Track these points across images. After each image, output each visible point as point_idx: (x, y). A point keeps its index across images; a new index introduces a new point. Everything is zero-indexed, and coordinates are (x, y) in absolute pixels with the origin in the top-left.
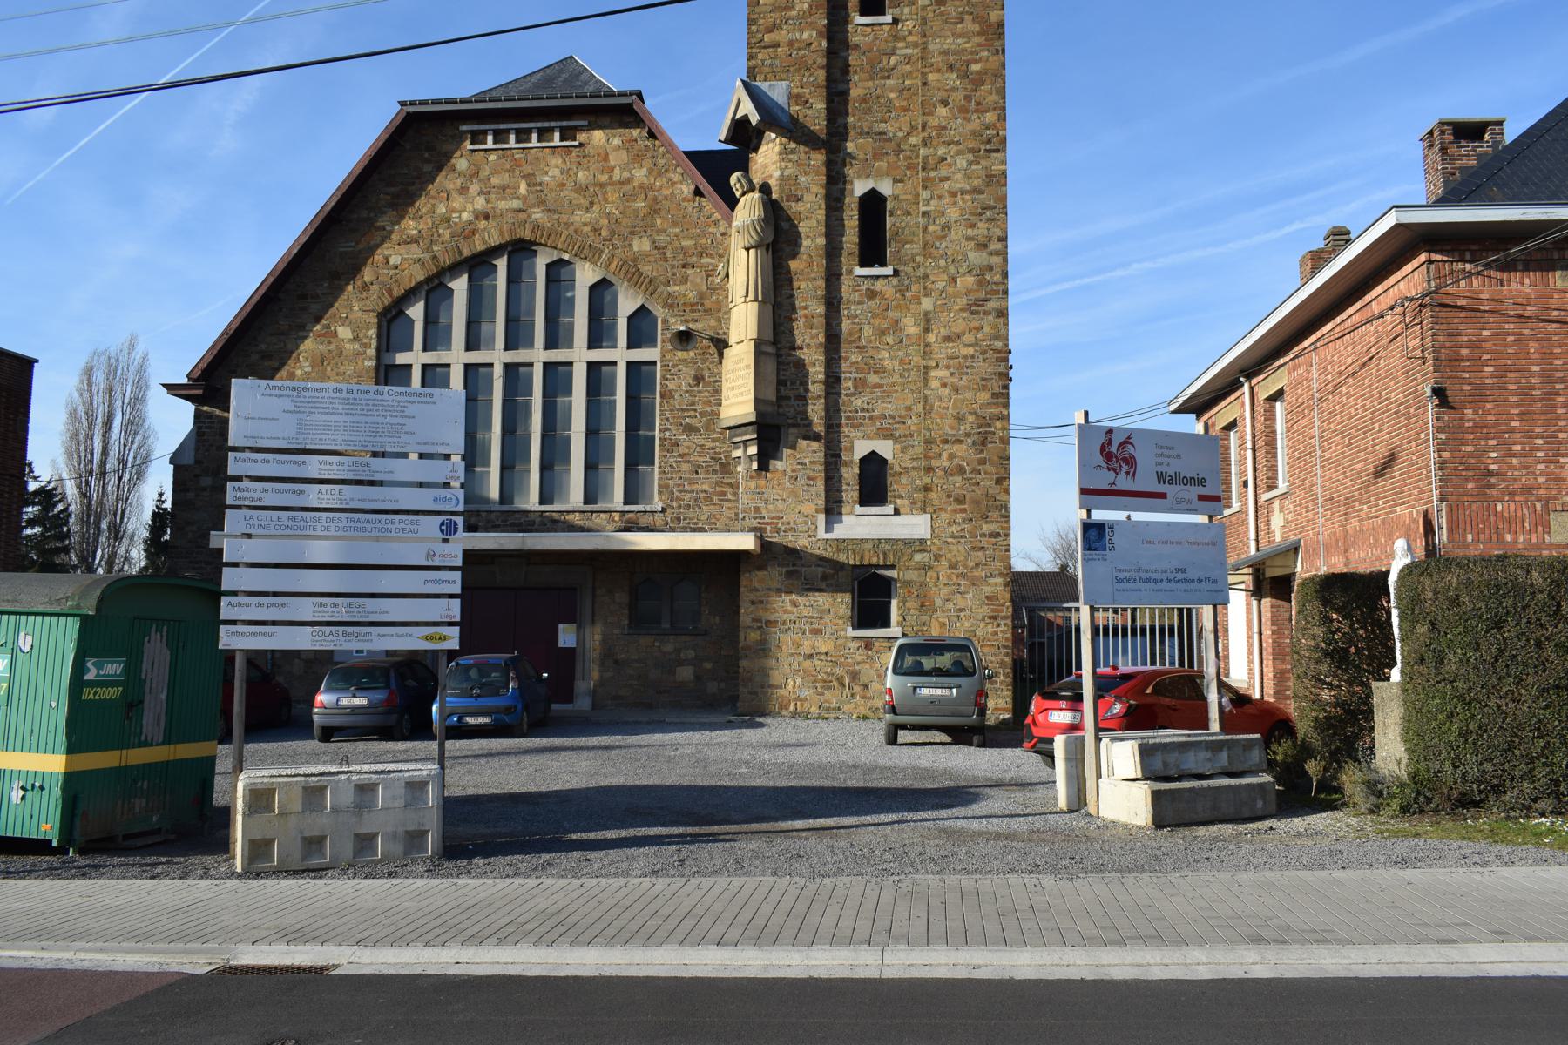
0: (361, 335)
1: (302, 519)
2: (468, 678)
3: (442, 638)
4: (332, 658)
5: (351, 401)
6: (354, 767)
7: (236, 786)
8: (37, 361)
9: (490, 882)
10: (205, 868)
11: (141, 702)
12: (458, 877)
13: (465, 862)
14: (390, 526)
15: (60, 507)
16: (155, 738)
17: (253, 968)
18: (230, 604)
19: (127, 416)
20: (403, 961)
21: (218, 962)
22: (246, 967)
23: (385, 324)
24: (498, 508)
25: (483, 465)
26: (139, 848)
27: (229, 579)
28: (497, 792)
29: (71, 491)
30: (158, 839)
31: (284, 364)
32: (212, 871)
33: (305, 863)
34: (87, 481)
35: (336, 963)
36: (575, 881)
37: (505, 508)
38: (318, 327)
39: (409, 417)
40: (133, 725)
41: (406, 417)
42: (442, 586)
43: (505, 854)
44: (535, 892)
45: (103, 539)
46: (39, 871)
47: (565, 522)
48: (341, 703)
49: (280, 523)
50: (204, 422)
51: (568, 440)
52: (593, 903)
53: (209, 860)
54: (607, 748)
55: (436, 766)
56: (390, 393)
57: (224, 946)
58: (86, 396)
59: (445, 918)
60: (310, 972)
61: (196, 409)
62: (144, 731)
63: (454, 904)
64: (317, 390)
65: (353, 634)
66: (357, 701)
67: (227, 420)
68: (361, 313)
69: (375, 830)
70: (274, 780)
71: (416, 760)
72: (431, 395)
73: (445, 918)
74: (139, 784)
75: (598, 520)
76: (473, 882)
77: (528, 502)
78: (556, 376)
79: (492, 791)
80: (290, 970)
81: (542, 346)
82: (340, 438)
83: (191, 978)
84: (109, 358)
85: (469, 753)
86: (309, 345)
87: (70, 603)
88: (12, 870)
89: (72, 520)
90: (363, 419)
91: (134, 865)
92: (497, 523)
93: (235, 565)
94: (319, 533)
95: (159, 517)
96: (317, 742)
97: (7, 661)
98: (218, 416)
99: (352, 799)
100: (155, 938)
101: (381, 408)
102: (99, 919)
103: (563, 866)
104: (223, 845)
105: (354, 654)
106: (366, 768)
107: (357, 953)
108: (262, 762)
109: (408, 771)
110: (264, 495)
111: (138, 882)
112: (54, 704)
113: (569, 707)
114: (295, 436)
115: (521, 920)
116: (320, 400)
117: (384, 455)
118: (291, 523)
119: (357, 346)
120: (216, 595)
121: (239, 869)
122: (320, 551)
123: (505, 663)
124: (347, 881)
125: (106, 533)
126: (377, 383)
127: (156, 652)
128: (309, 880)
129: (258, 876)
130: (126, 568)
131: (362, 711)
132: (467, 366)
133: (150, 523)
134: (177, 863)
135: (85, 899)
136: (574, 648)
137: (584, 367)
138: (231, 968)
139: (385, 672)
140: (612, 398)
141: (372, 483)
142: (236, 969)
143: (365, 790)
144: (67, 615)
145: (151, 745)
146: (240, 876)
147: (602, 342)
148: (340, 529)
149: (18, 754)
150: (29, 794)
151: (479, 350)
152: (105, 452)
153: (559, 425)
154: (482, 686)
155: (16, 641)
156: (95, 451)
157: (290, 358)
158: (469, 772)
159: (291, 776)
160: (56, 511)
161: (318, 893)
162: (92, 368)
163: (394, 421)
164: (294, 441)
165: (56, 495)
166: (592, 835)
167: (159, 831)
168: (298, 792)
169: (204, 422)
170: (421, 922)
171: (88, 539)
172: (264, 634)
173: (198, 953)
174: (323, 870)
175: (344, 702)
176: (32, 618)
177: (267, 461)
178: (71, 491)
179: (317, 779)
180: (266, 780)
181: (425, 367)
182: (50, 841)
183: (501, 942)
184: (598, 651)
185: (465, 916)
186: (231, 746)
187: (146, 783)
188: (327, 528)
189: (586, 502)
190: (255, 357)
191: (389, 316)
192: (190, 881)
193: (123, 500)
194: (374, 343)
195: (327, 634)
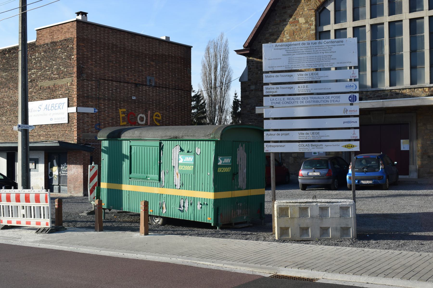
0: (308, 21)
1: (293, 99)
2: (361, 164)
3: (352, 146)
4: (304, 156)
5: (309, 48)
6: (319, 200)
7: (274, 206)
8: (192, 47)
9: (378, 250)
10: (264, 237)
11: (238, 173)
12: (364, 247)
13: (366, 242)
14: (328, 99)
15: (202, 101)
16: (243, 187)
17: (286, 277)
18: (267, 134)
19: (222, 65)
20: (345, 280)
21: (273, 273)
22: (283, 276)
23: (318, 14)
24: (371, 89)
25: (363, 71)
26: (240, 228)
27: (267, 124)
28: (377, 213)
29: (205, 95)
30: (247, 225)
31: (279, 37)
32: (267, 239)
33: (301, 238)
34: (210, 91)
35: (318, 278)
36: (417, 253)
37: (374, 89)
38: (291, 20)
39: (333, 52)
40: (235, 182)
41: (332, 52)
42: (352, 124)
43: (384, 239)
44: (399, 256)
45: (217, 113)
46: (208, 234)
47: (402, 94)
48: (309, 174)
49: (284, 101)
50: (251, 64)
51: (402, 56)
52: (427, 263)
53: (265, 234)
54: (426, 195)
55: (352, 201)
56: (325, 42)
57: (275, 267)
58: (208, 59)
59: (361, 264)
60: (308, 280)
61: (247, 59)
62: (239, 184)
63: (363, 258)
64: (295, 45)
65: (315, 145)
66: (316, 174)
67: (261, 63)
68: (308, 11)
69: (328, 226)
70: (288, 204)
71: (341, 198)
72: (342, 42)
73: (361, 264)
74: (239, 204)
75: (418, 92)
76: (371, 250)
77: (384, 86)
78: (303, 59)
79: (375, 212)
80: (300, 279)
81: (387, 15)
82: (306, 64)
83: (264, 278)
84: (215, 43)
85: (364, 196)
86: (288, 28)
87: (211, 136)
88: (200, 233)
89: (206, 106)
90: (314, 55)
91: (239, 234)
92: (371, 96)
93: (268, 119)
94: (299, 104)
95: (236, 103)
96: (300, 190)
97: (193, 158)
98: (255, 61)
99: (318, 213)
100: (250, 262)
101: (321, 49)
102: (230, 253)
103: (411, 246)
104: (270, 229)
105: (313, 154)
106: (323, 200)
107: (326, 275)
108: (281, 197)
109: (341, 202)
110: (277, 90)
111: (242, 241)
112: (209, 174)
113: (407, 177)
114: (288, 65)
115: (393, 268)
116: (297, 49)
117: (320, 69)
118: (288, 101)
119: (307, 25)
120: (261, 132)
121: (277, 239)
122: (301, 112)
123: (377, 157)
124: (318, 246)
125: (218, 111)
126: (316, 39)
127: (241, 153)
128: (303, 245)
129: (284, 241)
130: (225, 123)
131: (318, 178)
132: (354, 28)
133: (233, 105)
134: (254, 235)
135: (224, 246)
136: (408, 151)
137: (408, 21)
138: (278, 276)
139: (326, 161)
140: (422, 34)
141: (316, 82)
142: (280, 276)
143: (323, 209)
144: (211, 141)
145: (242, 190)
146: (277, 241)
147: (416, 8)
148: (308, 102)
149: (198, 192)
150: (203, 206)
151: (359, 20)
152: (215, 80)
153: (397, 50)
154: (367, 167)
155: (195, 151)
156: (212, 79)
157: (281, 34)
158: (364, 204)
159: (294, 203)
160: (201, 103)
161: (308, 249)
162: (209, 48)
163: (327, 54)
164: (287, 67)
165: (201, 97)
166: (423, 234)
167: (246, 222)
168: (297, 210)
169: (251, 64)
170: (350, 265)
171: (212, 113)
172: (281, 146)
173: (266, 269)
174: (309, 241)
175: (310, 174)
176: (199, 142)
177: (277, 76)
178: (205, 95)
179: (304, 204)
180: (285, 204)
181: (336, 30)
182: (211, 224)
183: (386, 276)
184: (420, 152)
185: (368, 264)
186: (271, 191)
187: (241, 204)
188: (303, 102)
189: (412, 84)
190: (267, 35)
191: (319, 11)
192: (259, 242)
193: (223, 97)
194: (314, 23)
195: (305, 146)
